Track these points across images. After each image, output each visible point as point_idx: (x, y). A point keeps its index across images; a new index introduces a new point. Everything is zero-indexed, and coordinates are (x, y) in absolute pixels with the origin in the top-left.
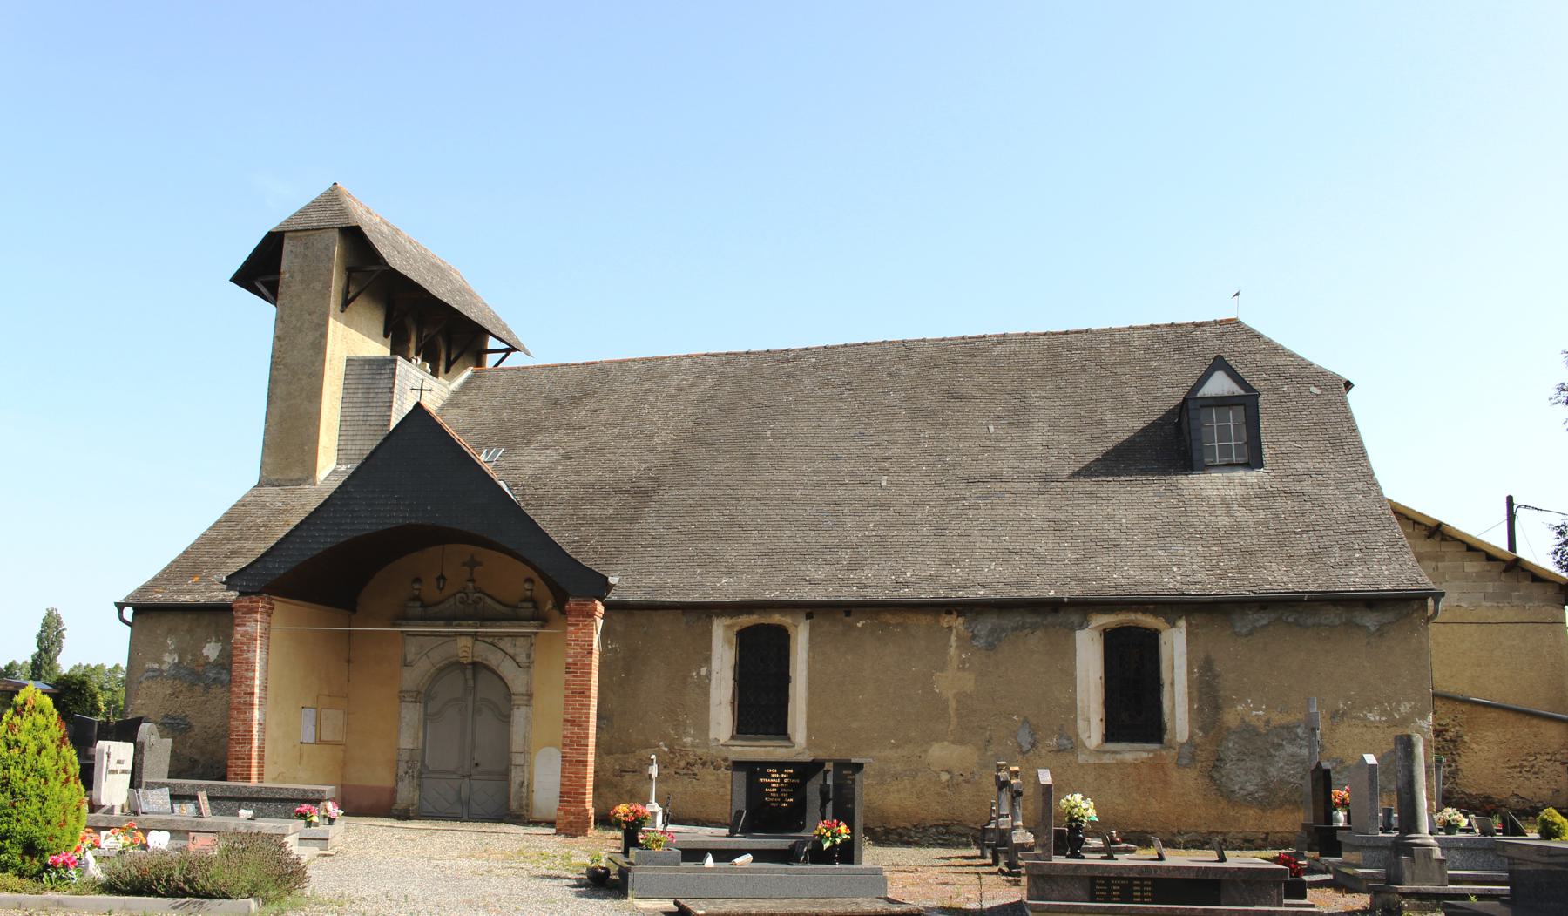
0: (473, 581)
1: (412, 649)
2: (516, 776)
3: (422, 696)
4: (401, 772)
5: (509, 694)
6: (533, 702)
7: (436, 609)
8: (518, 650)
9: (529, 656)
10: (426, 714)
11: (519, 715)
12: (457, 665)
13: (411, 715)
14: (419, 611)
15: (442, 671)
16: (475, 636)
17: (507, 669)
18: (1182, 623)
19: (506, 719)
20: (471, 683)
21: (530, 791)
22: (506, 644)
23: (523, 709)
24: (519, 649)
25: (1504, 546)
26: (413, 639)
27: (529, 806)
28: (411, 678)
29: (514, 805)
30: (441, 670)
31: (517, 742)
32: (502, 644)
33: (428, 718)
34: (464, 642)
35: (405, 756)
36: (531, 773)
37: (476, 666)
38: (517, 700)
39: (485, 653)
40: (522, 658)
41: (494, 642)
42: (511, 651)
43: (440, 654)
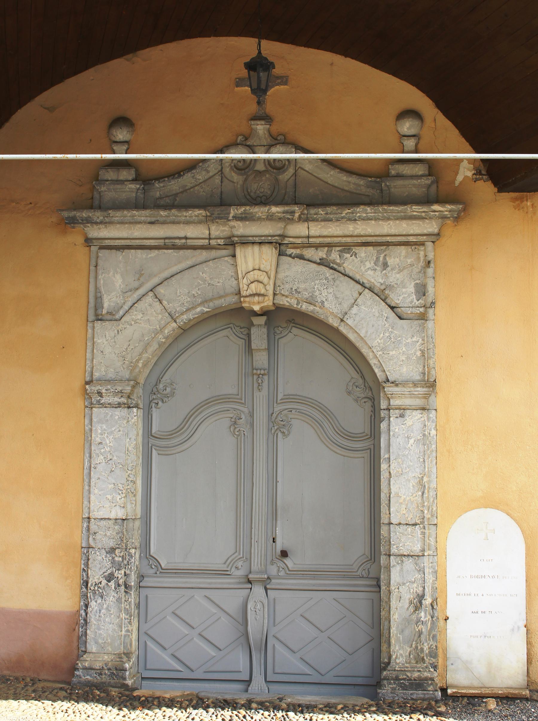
0: (267, 118)
1: (115, 279)
2: (403, 583)
3: (146, 392)
4: (96, 576)
5: (371, 389)
6: (438, 401)
7: (174, 185)
8: (394, 277)
9: (421, 291)
10: (148, 432)
11: (403, 435)
12: (237, 316)
13: (118, 433)
14: (132, 189)
15: (188, 333)
16: (280, 245)
17: (369, 326)
18: (457, 183)
19: (369, 448)
20: (261, 359)
21: (439, 619)
22: (362, 264)
23: (414, 419)
24: (399, 273)
25: (285, 561)
26: (120, 256)
27: (433, 654)
28: (115, 349)
29: (400, 653)
30: (185, 330)
31: (401, 495)
32: (350, 264)
33: (152, 442)
34: (250, 259)
35: (106, 537)
36: (439, 574)
37: (281, 318)
38: (399, 397)
39: (304, 284)
40: (405, 296)
41: (329, 258)
42: (375, 277)
43: (197, 284)
